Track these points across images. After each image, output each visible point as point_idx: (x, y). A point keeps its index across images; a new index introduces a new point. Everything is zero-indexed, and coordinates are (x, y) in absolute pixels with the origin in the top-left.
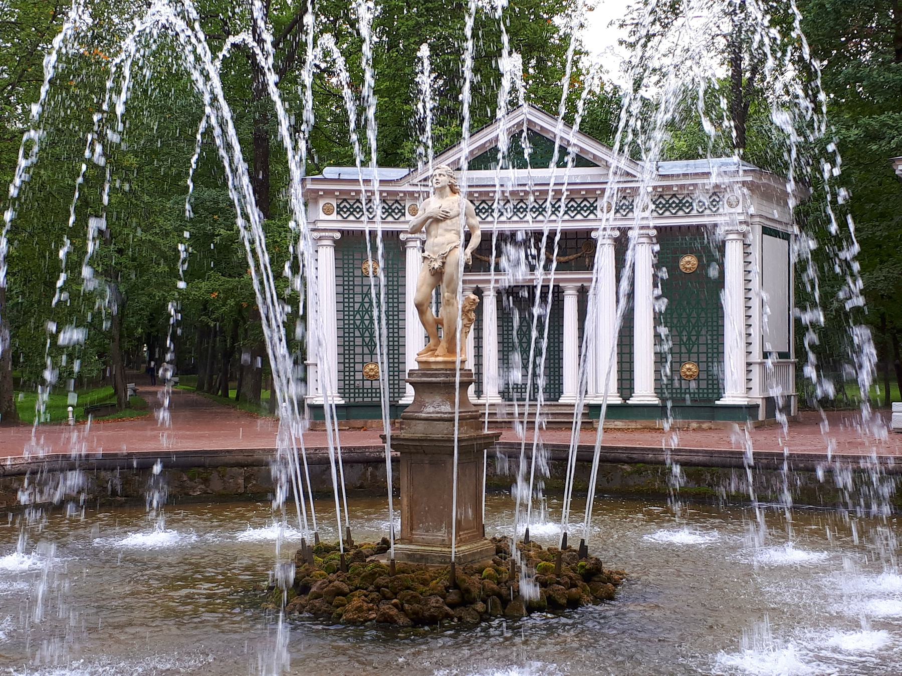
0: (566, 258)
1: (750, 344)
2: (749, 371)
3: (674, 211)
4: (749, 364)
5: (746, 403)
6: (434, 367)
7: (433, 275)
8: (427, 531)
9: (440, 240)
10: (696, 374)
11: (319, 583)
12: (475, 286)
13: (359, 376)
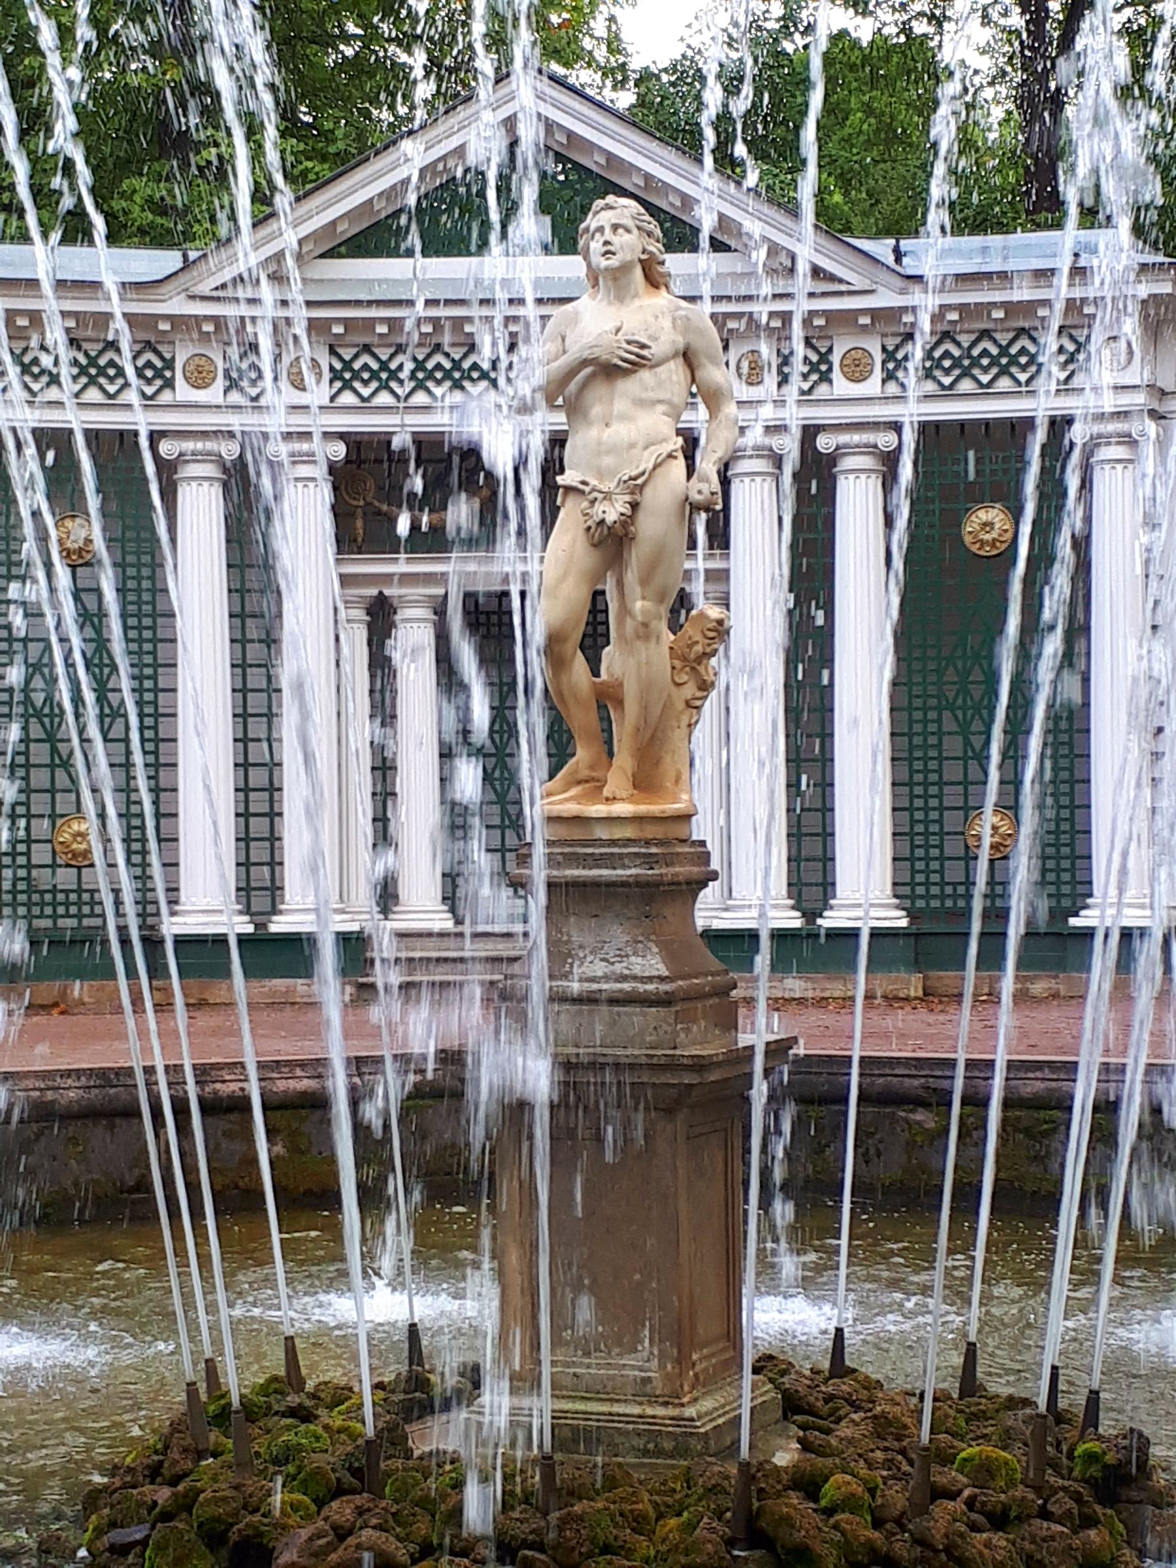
3: (985, 379)
6: (602, 833)
7: (594, 545)
8: (587, 1354)
9: (619, 432)
11: (304, 1534)
12: (374, 592)
13: (41, 853)
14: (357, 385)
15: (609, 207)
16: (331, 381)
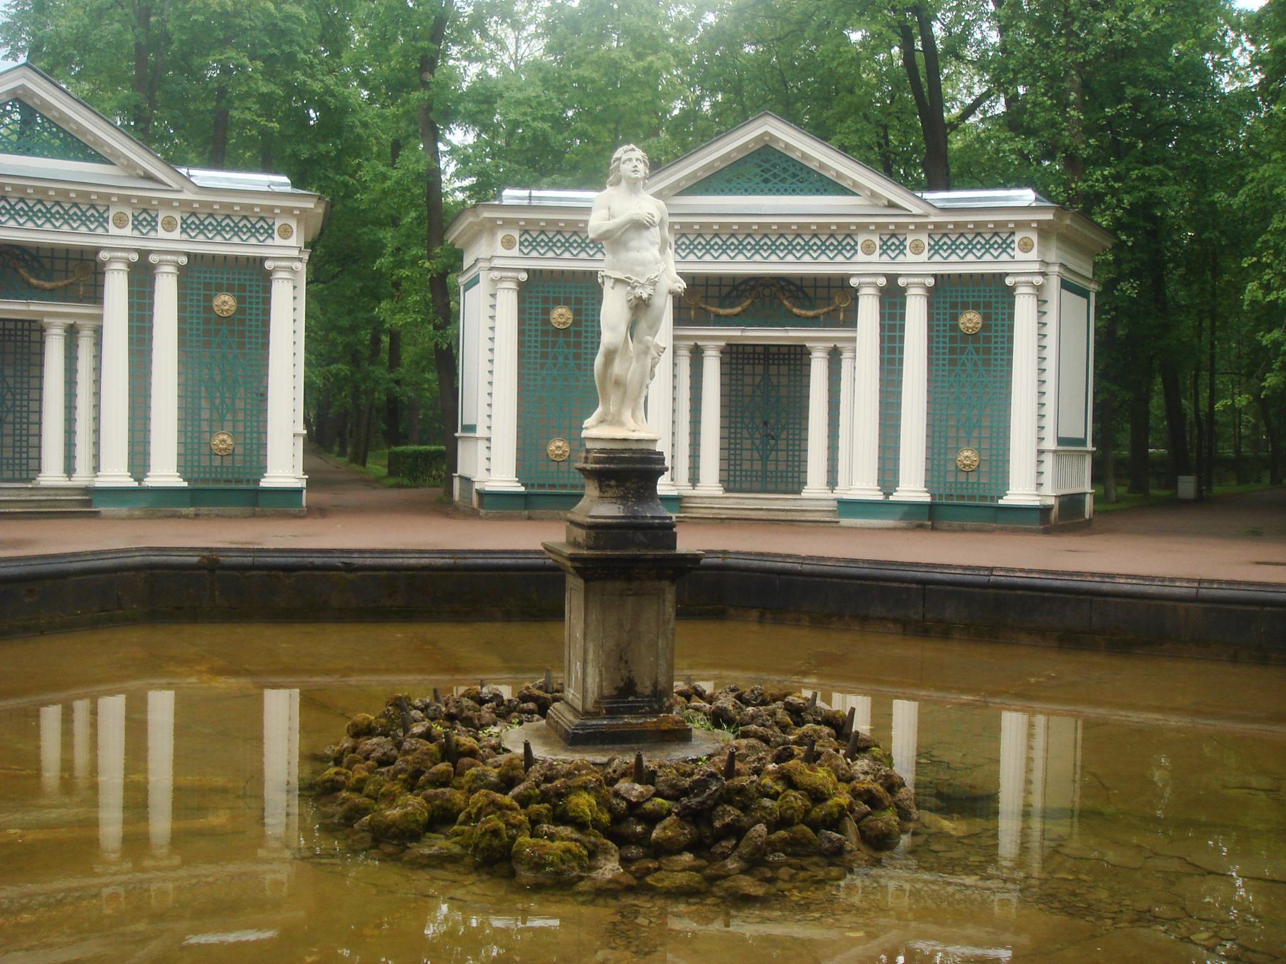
0: (816, 312)
1: (1043, 428)
2: (1040, 462)
3: (575, 252)
4: (1040, 452)
5: (1038, 503)
10: (567, 454)
12: (692, 343)
14: (889, 252)
15: (633, 150)
16: (929, 251)
